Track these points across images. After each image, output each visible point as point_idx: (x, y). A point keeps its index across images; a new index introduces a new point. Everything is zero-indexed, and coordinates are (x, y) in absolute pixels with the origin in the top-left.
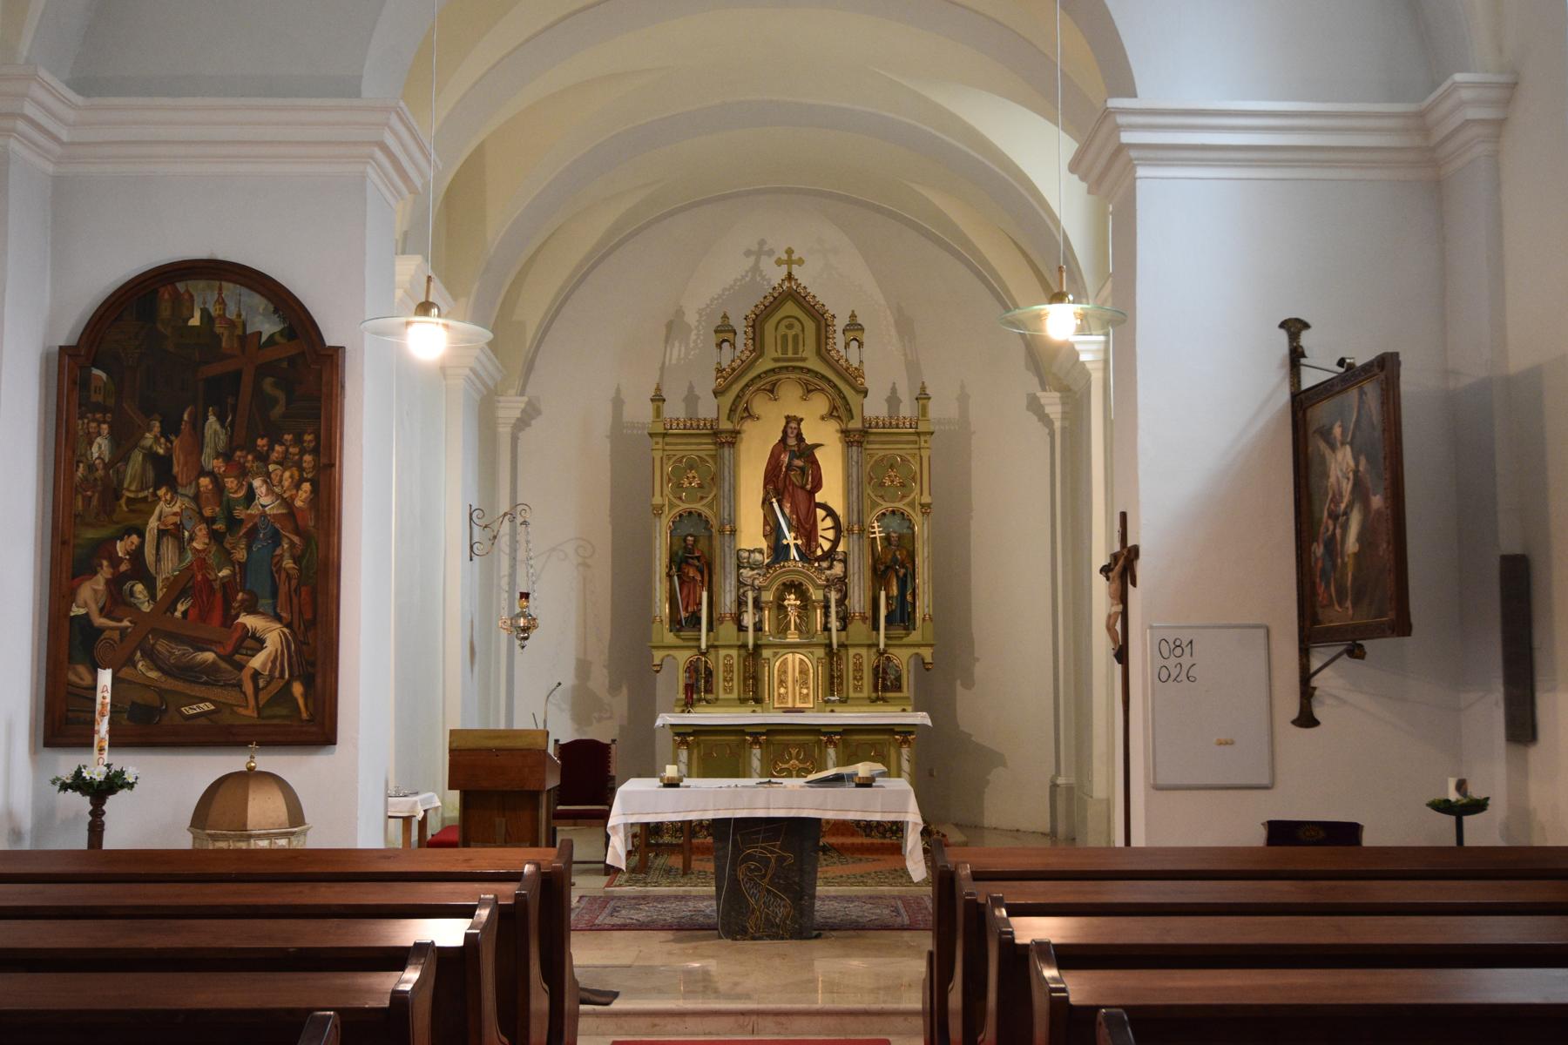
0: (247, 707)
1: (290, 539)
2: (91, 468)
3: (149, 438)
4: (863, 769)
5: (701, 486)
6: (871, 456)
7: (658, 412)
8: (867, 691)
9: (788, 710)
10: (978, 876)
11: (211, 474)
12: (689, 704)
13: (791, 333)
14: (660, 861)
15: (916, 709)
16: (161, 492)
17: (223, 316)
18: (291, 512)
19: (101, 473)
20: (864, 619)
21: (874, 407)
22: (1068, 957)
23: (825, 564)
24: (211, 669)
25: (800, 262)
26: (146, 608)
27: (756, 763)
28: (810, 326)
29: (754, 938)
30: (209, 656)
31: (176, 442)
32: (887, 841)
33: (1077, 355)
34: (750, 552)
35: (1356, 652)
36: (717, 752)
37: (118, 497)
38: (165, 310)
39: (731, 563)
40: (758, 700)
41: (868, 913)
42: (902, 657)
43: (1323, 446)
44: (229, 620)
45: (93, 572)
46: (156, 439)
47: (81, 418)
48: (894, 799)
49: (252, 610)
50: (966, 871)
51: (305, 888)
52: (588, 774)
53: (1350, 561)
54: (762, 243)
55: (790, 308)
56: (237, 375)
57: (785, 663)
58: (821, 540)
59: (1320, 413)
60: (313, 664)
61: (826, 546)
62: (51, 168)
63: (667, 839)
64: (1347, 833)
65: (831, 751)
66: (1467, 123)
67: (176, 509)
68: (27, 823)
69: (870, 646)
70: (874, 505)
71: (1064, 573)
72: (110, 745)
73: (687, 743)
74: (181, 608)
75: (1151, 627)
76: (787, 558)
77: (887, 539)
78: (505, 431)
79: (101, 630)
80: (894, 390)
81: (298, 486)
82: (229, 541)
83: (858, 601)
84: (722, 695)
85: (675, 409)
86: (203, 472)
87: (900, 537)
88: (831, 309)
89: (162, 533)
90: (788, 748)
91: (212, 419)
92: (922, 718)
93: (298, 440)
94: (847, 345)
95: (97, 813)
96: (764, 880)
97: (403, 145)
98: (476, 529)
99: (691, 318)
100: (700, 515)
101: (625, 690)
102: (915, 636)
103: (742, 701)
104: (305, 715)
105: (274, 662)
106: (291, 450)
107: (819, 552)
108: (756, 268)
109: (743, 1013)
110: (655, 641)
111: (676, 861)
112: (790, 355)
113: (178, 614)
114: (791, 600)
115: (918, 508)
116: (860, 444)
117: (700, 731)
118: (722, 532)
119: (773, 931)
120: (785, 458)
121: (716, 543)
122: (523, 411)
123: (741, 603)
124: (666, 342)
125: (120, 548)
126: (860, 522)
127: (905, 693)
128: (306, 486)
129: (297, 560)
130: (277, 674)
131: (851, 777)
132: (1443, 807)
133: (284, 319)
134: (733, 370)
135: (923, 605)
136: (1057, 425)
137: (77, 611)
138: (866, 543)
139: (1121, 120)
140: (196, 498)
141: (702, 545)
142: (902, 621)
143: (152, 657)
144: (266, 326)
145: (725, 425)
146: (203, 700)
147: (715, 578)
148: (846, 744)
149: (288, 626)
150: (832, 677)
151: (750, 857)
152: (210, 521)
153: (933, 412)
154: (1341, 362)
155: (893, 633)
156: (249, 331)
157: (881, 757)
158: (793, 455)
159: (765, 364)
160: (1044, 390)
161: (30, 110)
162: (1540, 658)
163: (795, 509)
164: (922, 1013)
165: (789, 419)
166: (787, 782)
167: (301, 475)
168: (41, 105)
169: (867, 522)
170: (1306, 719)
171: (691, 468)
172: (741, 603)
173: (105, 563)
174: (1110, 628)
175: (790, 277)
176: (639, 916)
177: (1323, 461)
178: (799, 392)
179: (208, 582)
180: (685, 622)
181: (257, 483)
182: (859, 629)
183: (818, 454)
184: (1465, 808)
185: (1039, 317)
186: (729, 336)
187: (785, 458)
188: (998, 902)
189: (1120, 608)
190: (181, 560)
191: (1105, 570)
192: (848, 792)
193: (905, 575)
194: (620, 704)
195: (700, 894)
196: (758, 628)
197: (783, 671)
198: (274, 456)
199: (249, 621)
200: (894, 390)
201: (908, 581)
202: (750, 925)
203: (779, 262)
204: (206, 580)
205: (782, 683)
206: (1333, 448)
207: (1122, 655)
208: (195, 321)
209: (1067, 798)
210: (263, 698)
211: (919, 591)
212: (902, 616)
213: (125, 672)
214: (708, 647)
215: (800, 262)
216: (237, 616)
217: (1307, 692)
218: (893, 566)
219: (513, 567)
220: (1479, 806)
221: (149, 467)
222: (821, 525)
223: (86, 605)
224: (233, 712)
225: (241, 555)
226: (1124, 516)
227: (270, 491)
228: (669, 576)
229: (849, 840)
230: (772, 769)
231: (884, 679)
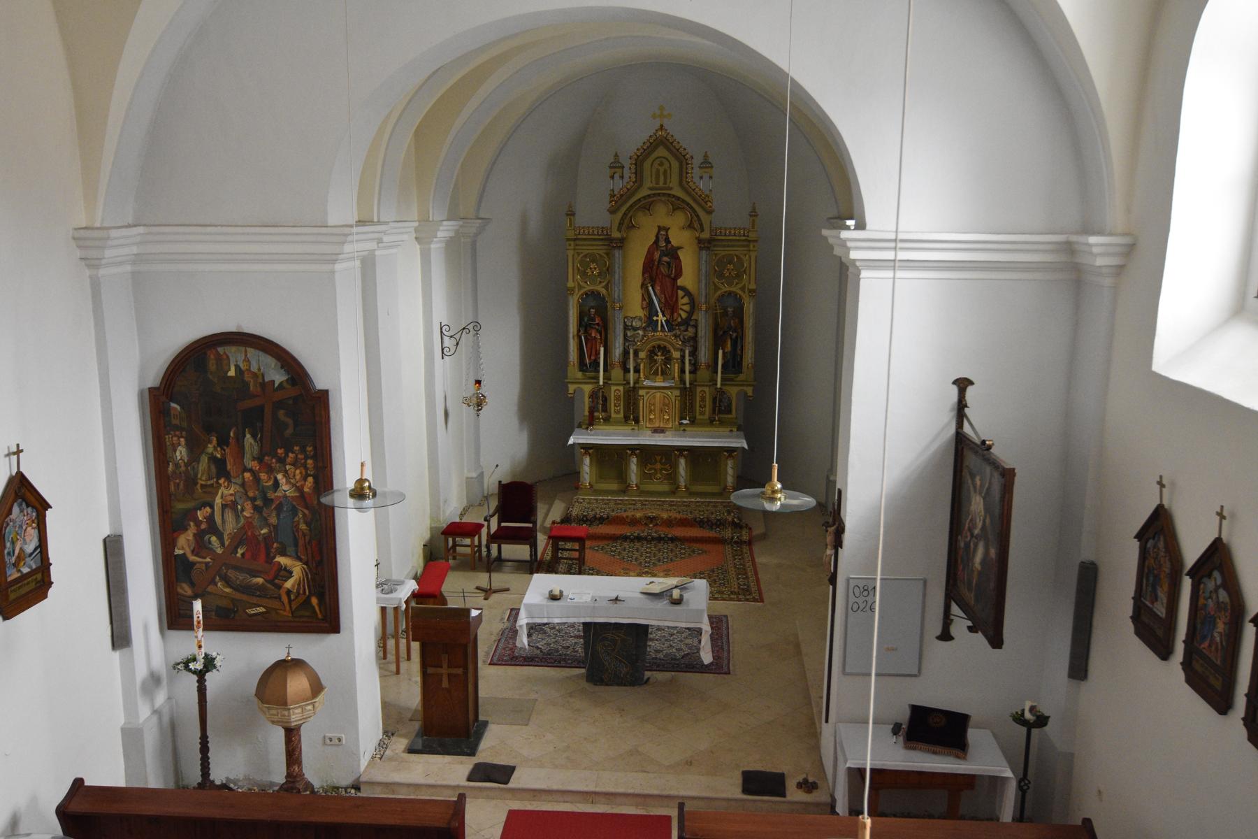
2: (177, 465)
3: (210, 448)
5: (600, 274)
9: (656, 431)
11: (250, 470)
16: (221, 481)
17: (249, 370)
18: (302, 495)
19: (183, 468)
26: (219, 551)
28: (675, 165)
30: (260, 580)
31: (227, 450)
38: (212, 365)
39: (620, 328)
42: (733, 391)
44: (269, 559)
45: (186, 529)
46: (215, 448)
49: (283, 554)
55: (661, 152)
61: (684, 315)
74: (240, 551)
81: (305, 479)
82: (265, 512)
83: (704, 355)
84: (613, 415)
86: (245, 470)
89: (224, 506)
91: (248, 436)
93: (303, 450)
98: (446, 339)
102: (742, 377)
113: (239, 555)
116: (708, 248)
119: (619, 681)
120: (657, 255)
123: (626, 353)
125: (200, 515)
127: (734, 415)
128: (310, 479)
129: (307, 523)
133: (288, 372)
135: (749, 357)
137: (178, 552)
140: (243, 485)
144: (277, 376)
145: (616, 234)
149: (306, 563)
152: (253, 500)
156: (267, 380)
158: (664, 254)
159: (644, 192)
163: (663, 291)
171: (593, 261)
180: (588, 366)
181: (280, 476)
182: (703, 374)
183: (680, 253)
187: (657, 255)
198: (289, 460)
201: (738, 342)
204: (253, 534)
208: (232, 373)
210: (294, 607)
212: (734, 365)
218: (728, 329)
221: (213, 467)
225: (273, 520)
227: (288, 482)
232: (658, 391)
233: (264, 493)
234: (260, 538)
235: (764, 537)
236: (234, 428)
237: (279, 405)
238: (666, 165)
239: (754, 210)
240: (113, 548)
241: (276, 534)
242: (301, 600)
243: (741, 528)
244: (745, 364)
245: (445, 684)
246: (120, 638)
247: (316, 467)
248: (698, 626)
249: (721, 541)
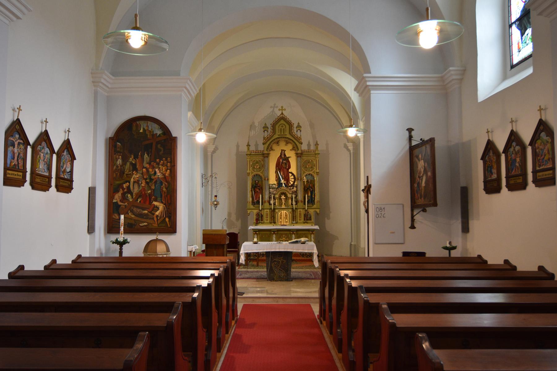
1: (165, 183)
2: (117, 166)
3: (131, 160)
4: (303, 239)
5: (259, 168)
7: (248, 149)
10: (332, 263)
11: (146, 168)
12: (257, 224)
14: (251, 263)
15: (315, 225)
20: (302, 202)
21: (304, 147)
22: (352, 278)
25: (285, 110)
26: (131, 200)
27: (274, 239)
28: (288, 126)
30: (146, 212)
35: (424, 211)
36: (265, 236)
37: (124, 174)
38: (134, 128)
40: (275, 223)
41: (304, 275)
42: (311, 211)
43: (417, 160)
44: (150, 203)
45: (118, 191)
48: (310, 247)
49: (156, 201)
50: (329, 261)
51: (178, 264)
52: (233, 242)
53: (423, 188)
54: (275, 104)
55: (282, 122)
56: (151, 144)
57: (281, 213)
59: (416, 152)
61: (292, 183)
62: (106, 94)
63: (252, 258)
64: (423, 254)
65: (293, 236)
66: (453, 80)
68: (104, 252)
70: (304, 172)
73: (256, 233)
74: (139, 200)
76: (282, 186)
77: (308, 181)
78: (209, 154)
79: (120, 206)
80: (309, 142)
81: (166, 171)
82: (150, 184)
83: (300, 197)
84: (265, 221)
85: (252, 148)
89: (134, 182)
90: (282, 235)
92: (317, 227)
93: (166, 160)
95: (121, 249)
96: (279, 266)
97: (191, 88)
99: (256, 124)
102: (315, 206)
103: (271, 223)
108: (273, 111)
109: (275, 298)
111: (255, 263)
114: (283, 197)
116: (300, 157)
118: (265, 180)
119: (281, 279)
120: (281, 160)
121: (264, 182)
123: (270, 198)
125: (125, 186)
126: (301, 177)
128: (169, 171)
129: (166, 189)
131: (300, 241)
132: (446, 248)
135: (317, 198)
136: (352, 151)
137: (114, 201)
139: (367, 79)
140: (142, 174)
141: (260, 183)
143: (132, 212)
144: (158, 132)
145: (266, 152)
148: (297, 234)
151: (275, 261)
152: (146, 179)
153: (320, 148)
154: (421, 139)
157: (306, 237)
158: (283, 160)
159: (276, 136)
161: (103, 81)
162: (470, 212)
163: (284, 174)
164: (319, 298)
165: (282, 150)
166: (284, 243)
168: (105, 79)
170: (413, 227)
172: (270, 198)
174: (364, 205)
175: (282, 114)
176: (246, 276)
177: (417, 164)
178: (285, 143)
179: (145, 194)
180: (255, 203)
181: (157, 170)
182: (300, 205)
183: (290, 159)
184: (451, 248)
185: (346, 131)
187: (281, 160)
188: (337, 267)
191: (363, 190)
192: (299, 245)
194: (239, 224)
195: (263, 271)
196: (274, 204)
197: (281, 215)
198: (161, 163)
199: (155, 203)
200: (309, 142)
201: (313, 192)
203: (279, 110)
205: (281, 218)
206: (419, 160)
207: (367, 211)
208: (141, 131)
209: (354, 248)
210: (159, 222)
211: (316, 195)
212: (312, 201)
213: (127, 216)
215: (285, 110)
217: (413, 220)
218: (309, 188)
219: (212, 189)
220: (454, 248)
222: (290, 178)
225: (153, 187)
226: (368, 177)
227: (160, 172)
228: (251, 191)
229: (298, 258)
230: (279, 239)
232: (283, 214)
233: (150, 176)
236: (142, 150)
237: (158, 143)
238: (284, 126)
240: (92, 191)
244: (316, 201)
246: (91, 229)
247: (171, 166)
248: (312, 251)
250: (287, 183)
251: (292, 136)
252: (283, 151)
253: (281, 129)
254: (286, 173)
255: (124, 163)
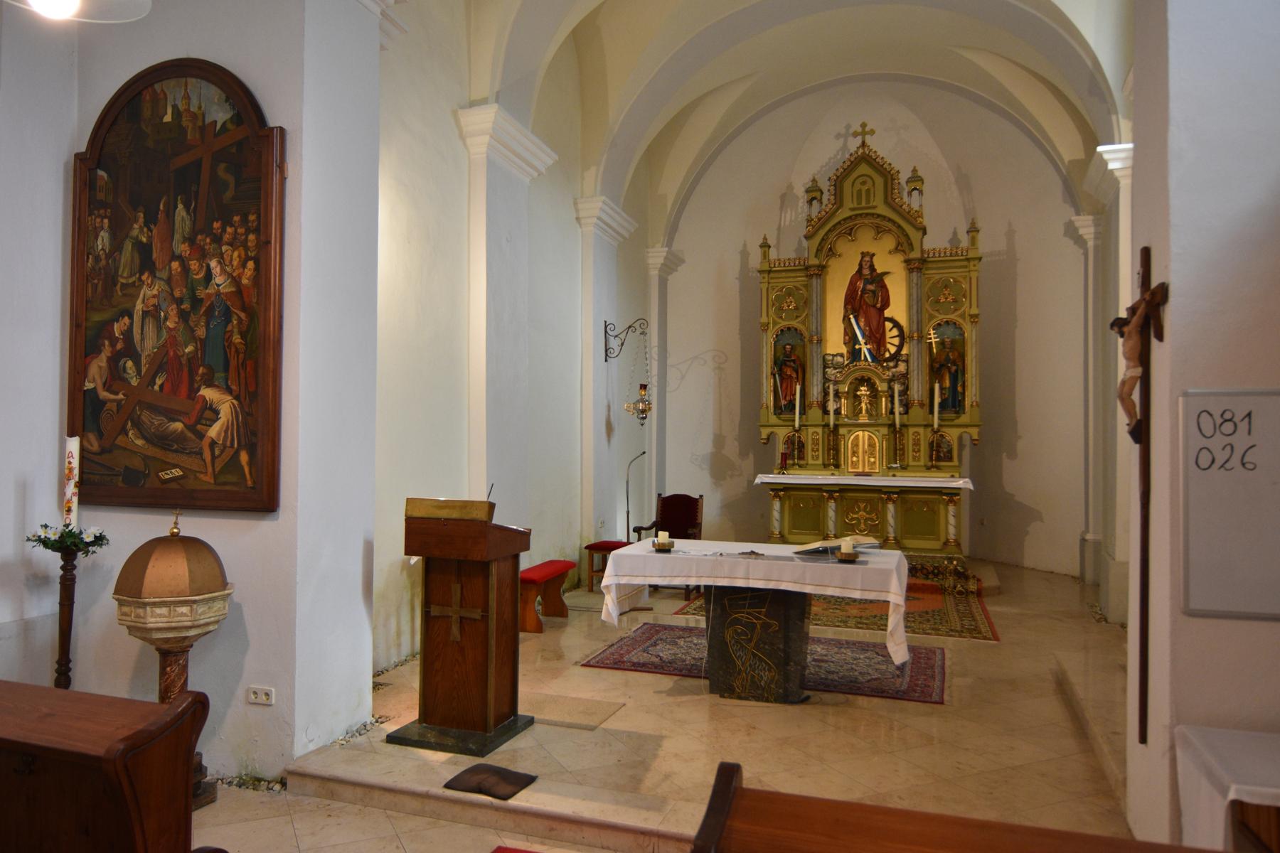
0: (206, 473)
2: (97, 259)
3: (135, 232)
4: (846, 544)
5: (796, 308)
6: (929, 279)
7: (765, 256)
8: (924, 458)
9: (858, 474)
11: (179, 258)
12: (784, 467)
13: (865, 188)
16: (144, 277)
17: (188, 110)
18: (239, 291)
19: (103, 262)
20: (922, 405)
21: (935, 241)
23: (891, 364)
24: (179, 438)
25: (872, 132)
26: (134, 382)
28: (879, 181)
29: (740, 698)
30: (178, 426)
31: (155, 231)
32: (929, 582)
33: (1105, 163)
34: (834, 356)
38: (147, 113)
40: (837, 466)
42: (952, 434)
44: (193, 392)
47: (90, 215)
49: (210, 384)
55: (864, 169)
56: (198, 164)
57: (857, 438)
58: (889, 346)
60: (254, 434)
61: (893, 350)
67: (155, 292)
69: (926, 426)
70: (931, 317)
71: (1095, 370)
72: (81, 502)
73: (776, 496)
74: (159, 382)
75: (1185, 394)
77: (942, 344)
78: (654, 273)
80: (955, 233)
81: (244, 266)
82: (193, 318)
83: (917, 391)
84: (811, 462)
86: (175, 257)
87: (953, 342)
88: (896, 165)
89: (145, 314)
91: (180, 206)
93: (245, 220)
94: (910, 193)
100: (789, 329)
101: (751, 456)
102: (964, 419)
103: (825, 466)
104: (250, 483)
105: (226, 432)
106: (239, 231)
107: (887, 355)
110: (763, 421)
112: (864, 204)
113: (156, 388)
114: (863, 390)
115: (968, 318)
116: (919, 270)
117: (788, 488)
118: (811, 341)
120: (860, 284)
121: (808, 351)
122: (666, 258)
123: (825, 393)
124: (781, 208)
125: (117, 329)
126: (920, 330)
128: (251, 264)
129: (243, 335)
130: (228, 444)
133: (233, 107)
134: (819, 219)
136: (1091, 244)
137: (89, 385)
138: (925, 347)
140: (169, 281)
141: (798, 352)
142: (954, 407)
143: (138, 425)
146: (175, 466)
147: (807, 376)
149: (237, 398)
150: (896, 450)
152: (179, 301)
155: (945, 416)
156: (208, 121)
158: (867, 282)
159: (844, 213)
160: (1078, 213)
163: (868, 323)
167: (246, 254)
169: (925, 332)
173: (107, 343)
175: (863, 144)
179: (177, 357)
180: (784, 408)
181: (213, 264)
182: (917, 413)
183: (888, 281)
186: (817, 194)
187: (860, 284)
189: (1138, 371)
190: (159, 337)
193: (956, 371)
197: (856, 444)
198: (226, 237)
199: (208, 393)
200: (955, 233)
201: (958, 375)
202: (737, 684)
205: (854, 453)
208: (168, 118)
210: (219, 465)
211: (968, 383)
212: (954, 403)
214: (800, 426)
215: (872, 132)
216: (199, 390)
218: (948, 364)
221: (136, 256)
222: (889, 334)
223: (94, 381)
224: (196, 478)
225: (201, 332)
227: (223, 271)
231: (938, 452)
233: (193, 290)
234: (184, 360)
235: (998, 591)
239: (973, 224)
241: (204, 352)
242: (229, 453)
243: (967, 578)
244: (968, 402)
245: (455, 630)
248: (882, 597)
249: (940, 591)
250: (879, 349)
251: (894, 209)
252: (867, 257)
253: (860, 192)
254: (874, 323)
255: (117, 246)
